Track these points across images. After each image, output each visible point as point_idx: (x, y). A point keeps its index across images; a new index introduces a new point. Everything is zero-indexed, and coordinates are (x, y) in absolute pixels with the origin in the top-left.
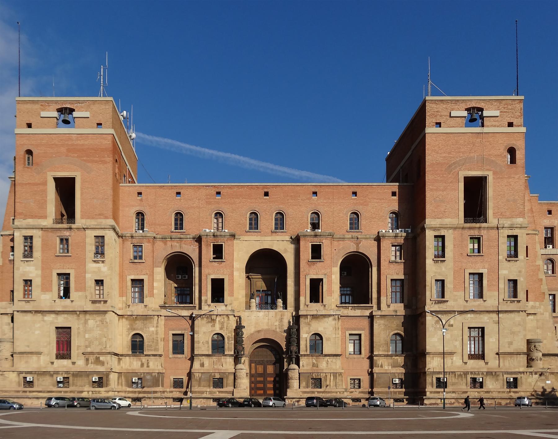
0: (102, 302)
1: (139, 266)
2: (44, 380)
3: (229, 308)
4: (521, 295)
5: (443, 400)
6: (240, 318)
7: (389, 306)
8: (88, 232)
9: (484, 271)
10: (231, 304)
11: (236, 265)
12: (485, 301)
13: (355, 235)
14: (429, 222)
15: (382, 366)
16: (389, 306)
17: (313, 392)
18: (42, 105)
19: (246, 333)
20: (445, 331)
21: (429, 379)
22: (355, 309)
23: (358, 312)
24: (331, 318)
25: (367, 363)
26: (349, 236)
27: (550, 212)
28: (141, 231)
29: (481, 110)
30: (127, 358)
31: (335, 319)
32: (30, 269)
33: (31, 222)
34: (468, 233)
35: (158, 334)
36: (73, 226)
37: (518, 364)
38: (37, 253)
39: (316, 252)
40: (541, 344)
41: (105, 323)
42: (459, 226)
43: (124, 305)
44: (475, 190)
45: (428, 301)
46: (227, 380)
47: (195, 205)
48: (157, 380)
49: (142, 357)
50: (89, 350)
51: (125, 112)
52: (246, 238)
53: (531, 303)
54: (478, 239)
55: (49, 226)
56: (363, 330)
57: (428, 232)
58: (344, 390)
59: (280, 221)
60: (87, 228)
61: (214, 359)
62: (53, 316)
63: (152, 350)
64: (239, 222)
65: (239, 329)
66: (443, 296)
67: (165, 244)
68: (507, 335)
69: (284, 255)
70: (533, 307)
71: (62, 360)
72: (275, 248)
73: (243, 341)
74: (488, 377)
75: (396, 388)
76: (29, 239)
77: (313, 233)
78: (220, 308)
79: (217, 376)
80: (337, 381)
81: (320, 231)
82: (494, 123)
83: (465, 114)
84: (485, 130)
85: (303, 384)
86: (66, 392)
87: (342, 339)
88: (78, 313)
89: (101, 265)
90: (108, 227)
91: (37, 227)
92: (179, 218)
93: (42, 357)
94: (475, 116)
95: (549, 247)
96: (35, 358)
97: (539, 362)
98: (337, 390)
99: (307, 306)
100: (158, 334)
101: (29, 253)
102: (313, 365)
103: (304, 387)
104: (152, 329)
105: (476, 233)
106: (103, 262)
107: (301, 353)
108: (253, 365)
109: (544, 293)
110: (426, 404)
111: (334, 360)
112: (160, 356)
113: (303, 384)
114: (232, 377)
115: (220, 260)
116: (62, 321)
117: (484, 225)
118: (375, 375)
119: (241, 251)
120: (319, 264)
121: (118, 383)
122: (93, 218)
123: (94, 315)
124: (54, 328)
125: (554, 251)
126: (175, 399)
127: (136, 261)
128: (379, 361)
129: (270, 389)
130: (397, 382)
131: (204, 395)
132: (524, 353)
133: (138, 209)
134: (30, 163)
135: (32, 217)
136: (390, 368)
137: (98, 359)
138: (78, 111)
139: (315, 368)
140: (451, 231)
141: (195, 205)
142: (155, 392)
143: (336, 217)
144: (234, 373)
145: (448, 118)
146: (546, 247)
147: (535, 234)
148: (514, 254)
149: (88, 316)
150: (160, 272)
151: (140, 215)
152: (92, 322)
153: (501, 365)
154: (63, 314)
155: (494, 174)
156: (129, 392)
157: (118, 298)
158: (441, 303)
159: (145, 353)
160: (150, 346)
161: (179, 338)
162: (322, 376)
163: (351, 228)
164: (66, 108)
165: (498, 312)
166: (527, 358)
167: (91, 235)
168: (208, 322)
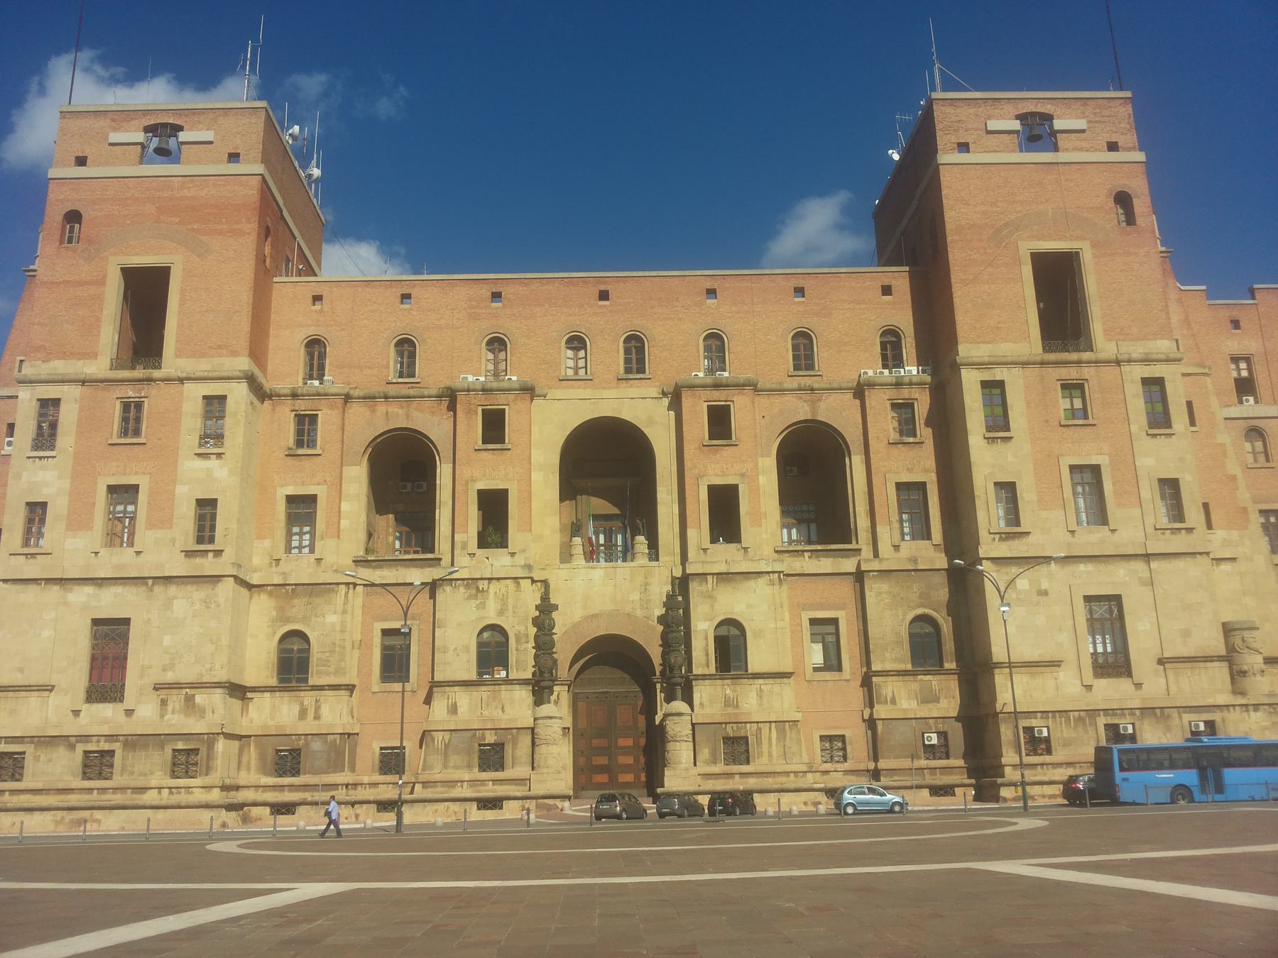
0: (211, 555)
1: (307, 463)
2: (50, 760)
3: (520, 560)
4: (1194, 516)
5: (1020, 789)
6: (545, 583)
7: (896, 548)
8: (188, 386)
9: (1101, 460)
10: (524, 551)
11: (537, 456)
12: (1113, 531)
13: (807, 382)
14: (966, 350)
15: (893, 701)
16: (896, 548)
17: (730, 775)
18: (113, 120)
19: (562, 622)
20: (1006, 609)
21: (1006, 732)
22: (818, 557)
23: (826, 565)
24: (762, 581)
25: (857, 695)
26: (794, 383)
27: (1236, 324)
28: (316, 383)
29: (1048, 118)
30: (267, 695)
31: (772, 583)
32: (47, 479)
33: (60, 366)
34: (1055, 375)
35: (344, 632)
36: (156, 374)
37: (1210, 685)
38: (66, 439)
39: (720, 422)
40: (1256, 633)
41: (213, 606)
42: (1033, 359)
43: (267, 561)
44: (1058, 283)
45: (983, 534)
46: (514, 749)
47: (442, 322)
48: (341, 748)
49: (302, 694)
50: (170, 677)
51: (296, 129)
52: (559, 393)
53: (1219, 534)
54: (1073, 388)
55: (100, 376)
56: (841, 609)
57: (965, 373)
58: (805, 769)
59: (636, 354)
60: (189, 379)
61: (484, 692)
62: (89, 590)
63: (328, 674)
64: (553, 352)
65: (546, 608)
66: (1017, 522)
67: (373, 411)
68: (1174, 612)
69: (646, 431)
70: (1226, 543)
71: (101, 706)
72: (626, 415)
73: (553, 644)
74: (1146, 722)
75: (934, 758)
76: (49, 406)
77: (709, 380)
78: (498, 562)
79: (491, 738)
80: (788, 743)
81: (726, 374)
82: (1078, 144)
83: (1016, 125)
84: (1061, 157)
85: (705, 754)
86: (103, 790)
87: (793, 632)
88: (150, 582)
89: (213, 463)
90: (238, 374)
91: (73, 377)
92: (406, 347)
93: (53, 699)
94: (1037, 132)
95: (1247, 401)
96: (34, 699)
97: (1258, 678)
98: (789, 768)
99: (705, 550)
100: (344, 632)
101: (46, 437)
102: (728, 702)
103: (707, 763)
104: (332, 619)
105: (1071, 373)
106: (219, 455)
107: (695, 672)
108: (581, 705)
109: (1245, 510)
110: (1005, 800)
111: (776, 688)
112: (351, 688)
113: (705, 754)
114: (526, 740)
115: (498, 446)
116: (110, 603)
117: (1086, 356)
118: (880, 725)
119: (545, 430)
120: (728, 452)
121: (240, 763)
122: (203, 355)
123: (189, 588)
124: (89, 622)
125: (1261, 410)
126: (384, 806)
127: (300, 451)
128: (888, 687)
129: (627, 769)
130: (935, 741)
131: (457, 792)
132: (1220, 658)
133: (311, 331)
134: (69, 239)
135: (64, 355)
136: (914, 704)
137: (189, 699)
138: (191, 130)
139: (730, 710)
140: (1016, 371)
141: (442, 322)
142: (334, 786)
143: (759, 341)
144: (533, 729)
145: (983, 133)
146: (1241, 402)
147: (1204, 374)
148: (1160, 420)
149: (173, 589)
150: (357, 478)
151: (315, 347)
152: (184, 602)
153: (1173, 689)
154: (114, 584)
155: (1093, 246)
156: (266, 788)
157: (253, 544)
158: (1013, 538)
159: (311, 682)
160: (325, 663)
161: (396, 641)
162: (750, 730)
163: (797, 368)
164: (165, 125)
165: (1147, 557)
166: (1231, 668)
167: (195, 393)
168: (471, 597)
